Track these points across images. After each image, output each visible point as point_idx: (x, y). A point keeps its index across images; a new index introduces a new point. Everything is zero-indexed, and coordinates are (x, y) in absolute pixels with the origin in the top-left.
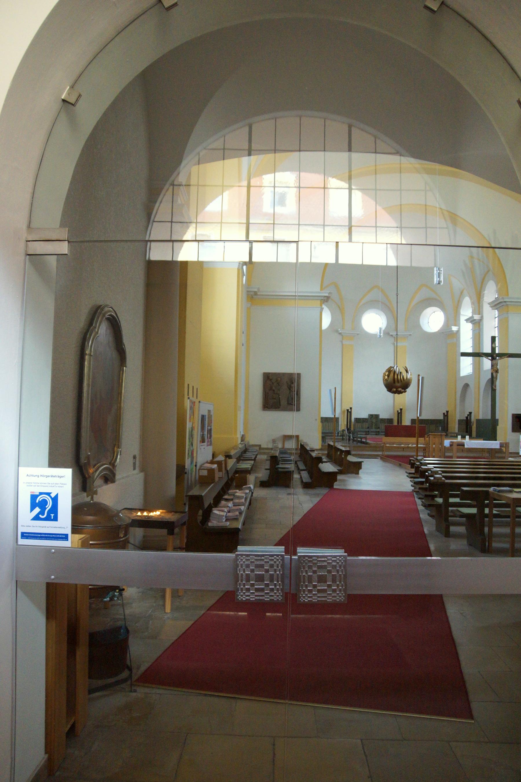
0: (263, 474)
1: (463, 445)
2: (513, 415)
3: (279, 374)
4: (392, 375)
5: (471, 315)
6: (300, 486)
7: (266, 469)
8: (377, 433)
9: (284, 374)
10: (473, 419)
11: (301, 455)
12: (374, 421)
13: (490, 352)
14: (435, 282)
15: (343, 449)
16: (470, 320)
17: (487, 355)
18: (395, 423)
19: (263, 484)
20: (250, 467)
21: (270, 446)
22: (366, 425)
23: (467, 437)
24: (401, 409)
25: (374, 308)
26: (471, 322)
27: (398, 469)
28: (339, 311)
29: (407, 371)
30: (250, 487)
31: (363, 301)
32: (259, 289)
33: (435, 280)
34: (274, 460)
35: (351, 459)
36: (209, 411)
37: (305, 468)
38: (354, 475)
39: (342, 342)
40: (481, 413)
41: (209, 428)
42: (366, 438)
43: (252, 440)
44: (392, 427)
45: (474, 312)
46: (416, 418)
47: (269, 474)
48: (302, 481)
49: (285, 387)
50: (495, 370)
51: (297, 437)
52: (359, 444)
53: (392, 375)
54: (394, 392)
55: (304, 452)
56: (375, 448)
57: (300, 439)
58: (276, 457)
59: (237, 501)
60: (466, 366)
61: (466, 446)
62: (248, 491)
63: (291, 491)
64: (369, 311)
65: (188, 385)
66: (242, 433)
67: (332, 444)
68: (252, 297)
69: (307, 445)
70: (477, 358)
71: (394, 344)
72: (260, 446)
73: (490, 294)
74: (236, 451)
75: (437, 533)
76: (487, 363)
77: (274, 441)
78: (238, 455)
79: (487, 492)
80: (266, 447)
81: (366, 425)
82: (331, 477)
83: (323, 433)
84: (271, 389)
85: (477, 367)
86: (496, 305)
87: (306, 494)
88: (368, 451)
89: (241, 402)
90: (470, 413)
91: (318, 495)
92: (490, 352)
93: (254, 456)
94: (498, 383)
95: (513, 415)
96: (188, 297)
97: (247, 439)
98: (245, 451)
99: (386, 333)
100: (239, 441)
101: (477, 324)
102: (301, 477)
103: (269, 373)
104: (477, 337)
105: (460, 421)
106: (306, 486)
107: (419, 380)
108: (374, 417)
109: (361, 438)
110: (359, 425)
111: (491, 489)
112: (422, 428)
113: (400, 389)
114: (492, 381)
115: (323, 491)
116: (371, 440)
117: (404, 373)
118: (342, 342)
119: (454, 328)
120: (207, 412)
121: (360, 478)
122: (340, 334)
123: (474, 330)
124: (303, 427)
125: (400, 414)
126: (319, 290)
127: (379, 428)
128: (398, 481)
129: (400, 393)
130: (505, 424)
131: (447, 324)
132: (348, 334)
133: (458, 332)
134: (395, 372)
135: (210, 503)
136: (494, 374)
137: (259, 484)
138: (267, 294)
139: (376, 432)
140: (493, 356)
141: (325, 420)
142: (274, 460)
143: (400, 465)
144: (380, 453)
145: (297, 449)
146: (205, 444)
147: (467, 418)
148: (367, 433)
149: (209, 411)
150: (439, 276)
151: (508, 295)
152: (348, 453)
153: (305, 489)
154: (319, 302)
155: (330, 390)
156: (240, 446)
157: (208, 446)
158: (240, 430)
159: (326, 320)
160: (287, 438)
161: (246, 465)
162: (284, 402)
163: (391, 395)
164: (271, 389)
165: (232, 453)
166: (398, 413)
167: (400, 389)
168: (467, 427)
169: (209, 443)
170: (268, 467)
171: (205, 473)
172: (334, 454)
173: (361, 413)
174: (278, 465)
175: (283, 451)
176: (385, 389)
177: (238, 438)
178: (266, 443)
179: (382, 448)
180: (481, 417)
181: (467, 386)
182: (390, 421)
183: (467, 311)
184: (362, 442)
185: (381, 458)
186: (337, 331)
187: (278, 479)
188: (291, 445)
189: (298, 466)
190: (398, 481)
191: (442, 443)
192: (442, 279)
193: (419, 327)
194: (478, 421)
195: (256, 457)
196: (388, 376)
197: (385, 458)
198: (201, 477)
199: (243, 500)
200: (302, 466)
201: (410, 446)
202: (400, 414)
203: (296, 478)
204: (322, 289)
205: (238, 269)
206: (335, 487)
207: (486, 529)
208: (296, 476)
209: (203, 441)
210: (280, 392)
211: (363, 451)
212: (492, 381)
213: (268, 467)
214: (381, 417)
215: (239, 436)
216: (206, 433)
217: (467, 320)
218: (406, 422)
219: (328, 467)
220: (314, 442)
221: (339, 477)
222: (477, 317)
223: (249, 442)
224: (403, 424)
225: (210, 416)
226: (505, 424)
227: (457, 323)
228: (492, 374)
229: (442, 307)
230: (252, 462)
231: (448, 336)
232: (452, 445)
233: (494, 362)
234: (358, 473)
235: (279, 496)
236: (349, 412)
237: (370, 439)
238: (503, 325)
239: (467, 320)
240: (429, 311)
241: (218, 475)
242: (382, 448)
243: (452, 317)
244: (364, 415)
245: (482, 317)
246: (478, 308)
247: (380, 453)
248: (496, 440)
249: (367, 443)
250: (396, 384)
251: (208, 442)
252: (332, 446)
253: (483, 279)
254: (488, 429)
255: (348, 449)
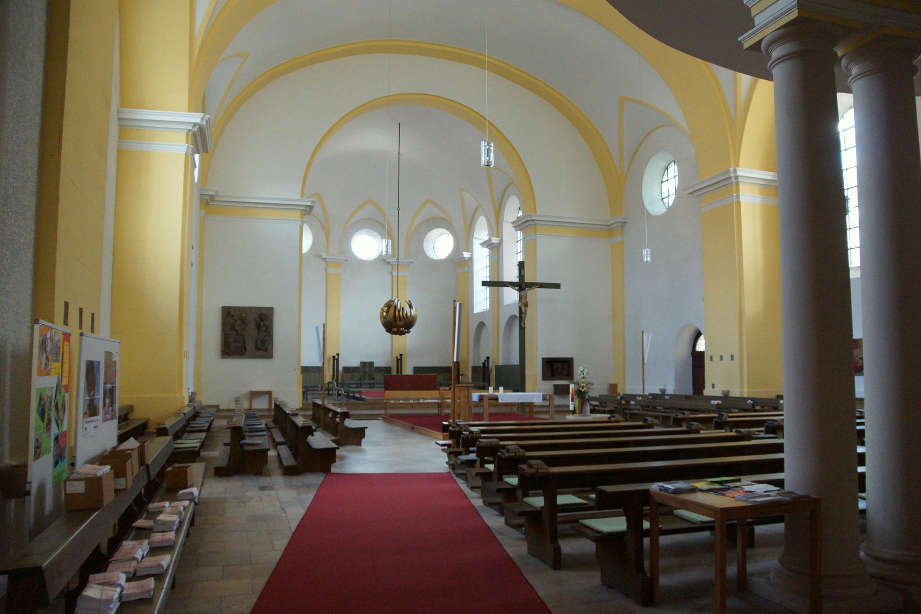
0: (219, 453)
1: (496, 399)
2: (543, 359)
3: (244, 308)
4: (392, 310)
5: (486, 238)
6: (279, 471)
7: (226, 445)
8: (372, 386)
9: (250, 308)
10: (491, 365)
11: (275, 420)
12: (367, 370)
13: (517, 280)
14: (483, 163)
15: (339, 410)
16: (487, 244)
17: (512, 284)
18: (394, 373)
19: (222, 473)
20: (198, 445)
21: (232, 406)
22: (357, 375)
23: (501, 388)
24: (401, 355)
25: (365, 228)
26: (487, 247)
27: (410, 434)
28: (323, 229)
29: (411, 307)
30: (192, 493)
31: (352, 221)
32: (217, 192)
33: (483, 159)
34: (237, 432)
35: (350, 423)
36: (109, 355)
37: (282, 440)
38: (354, 447)
39: (326, 270)
40: (501, 355)
41: (109, 386)
42: (360, 393)
43: (205, 399)
44: (390, 378)
45: (491, 235)
46: (451, 365)
47: (229, 452)
48: (281, 463)
49: (252, 326)
50: (523, 304)
51: (269, 393)
52: (352, 401)
53: (392, 310)
54: (396, 333)
55: (280, 416)
56: (373, 405)
57: (274, 396)
58: (240, 428)
59: (157, 537)
60: (481, 300)
61: (500, 401)
62: (187, 503)
63: (264, 481)
64: (360, 232)
65: (81, 310)
66: (191, 390)
67: (319, 402)
68: (208, 204)
69: (285, 405)
70: (495, 288)
71: (391, 273)
72: (218, 406)
73: (512, 211)
74: (178, 419)
75: (534, 560)
76: (511, 296)
77: (237, 400)
78: (178, 428)
79: (647, 492)
80: (226, 407)
81: (357, 375)
82: (327, 457)
83: (303, 387)
84: (233, 328)
85: (496, 301)
86: (520, 225)
87: (291, 487)
88: (365, 409)
89: (189, 346)
90: (488, 358)
91: (308, 487)
92: (517, 280)
93: (207, 424)
94: (528, 321)
95: (543, 359)
96: (64, 128)
97: (197, 398)
98: (196, 415)
99: (382, 260)
100: (186, 402)
101: (495, 249)
102: (279, 455)
103: (230, 308)
104: (496, 262)
105: (475, 369)
106: (289, 471)
107: (455, 308)
108: (367, 367)
109: (354, 392)
110: (349, 375)
111: (655, 487)
112: (426, 378)
113: (402, 329)
114: (522, 315)
115: (317, 479)
116: (367, 394)
117: (407, 309)
118: (326, 270)
119: (466, 255)
120: (103, 354)
121: (364, 451)
122: (324, 259)
123: (491, 257)
124: (276, 380)
125: (399, 361)
126: (298, 197)
127: (373, 379)
128: (428, 455)
129: (402, 333)
130: (534, 370)
131: (457, 249)
132: (334, 260)
133: (471, 259)
134: (395, 307)
135: (141, 493)
136: (523, 308)
137: (212, 471)
138: (228, 199)
139: (370, 384)
140: (521, 286)
141: (305, 370)
142: (237, 432)
143: (413, 428)
144: (382, 412)
145: (269, 410)
146: (100, 417)
147: (484, 364)
148: (359, 386)
149: (109, 355)
150: (488, 155)
151: (536, 212)
152: (345, 415)
153: (288, 478)
154: (299, 213)
155: (317, 328)
156: (187, 410)
157: (105, 420)
158: (189, 386)
159: (307, 243)
160: (254, 395)
161: (191, 442)
162: (250, 346)
163: (389, 335)
164: (233, 328)
165: (168, 424)
166: (398, 360)
167: (402, 329)
168: (483, 375)
169: (109, 416)
170: (228, 441)
171: (79, 488)
172: (323, 418)
173: (350, 360)
174: (243, 439)
175: (251, 415)
176: (384, 329)
177: (183, 397)
178: (225, 403)
179: (385, 406)
180: (501, 363)
181: (482, 325)
182: (388, 369)
183: (481, 234)
184: (354, 398)
185: (384, 419)
186: (320, 256)
187: (244, 462)
188: (261, 404)
189: (272, 435)
190: (428, 455)
191: (469, 397)
192: (492, 159)
193: (423, 252)
194: (498, 368)
195: (211, 424)
196: (387, 312)
197: (391, 419)
198: (71, 497)
199: (172, 535)
200: (279, 438)
201: (421, 401)
202: (399, 361)
203: (273, 457)
204: (302, 196)
205: (186, 155)
206: (333, 470)
207: (647, 564)
208: (272, 453)
209: (92, 411)
210: (247, 332)
211: (356, 409)
212: (522, 315)
213: (228, 441)
214: (376, 365)
215: (186, 396)
216: (100, 396)
217: (482, 244)
218: (408, 370)
219: (320, 440)
220: (292, 399)
221: (338, 452)
222: (495, 240)
223: (201, 403)
224: (404, 373)
225: (110, 365)
226: (534, 370)
227: (469, 248)
228: (520, 308)
229: (449, 226)
230: (203, 435)
231: (459, 264)
232: (481, 398)
233: (523, 293)
234: (360, 445)
235: (247, 494)
236: (336, 359)
237: (367, 393)
238: (530, 247)
239: (482, 244)
240: (435, 232)
241: (108, 496)
242: (385, 406)
243: (464, 241)
244: (355, 363)
245: (502, 240)
246: (496, 227)
247: (382, 412)
248: (524, 391)
249: (360, 399)
250: (397, 322)
251: (105, 413)
252: (319, 405)
253: (474, 214)
254: (514, 378)
255: (345, 410)
